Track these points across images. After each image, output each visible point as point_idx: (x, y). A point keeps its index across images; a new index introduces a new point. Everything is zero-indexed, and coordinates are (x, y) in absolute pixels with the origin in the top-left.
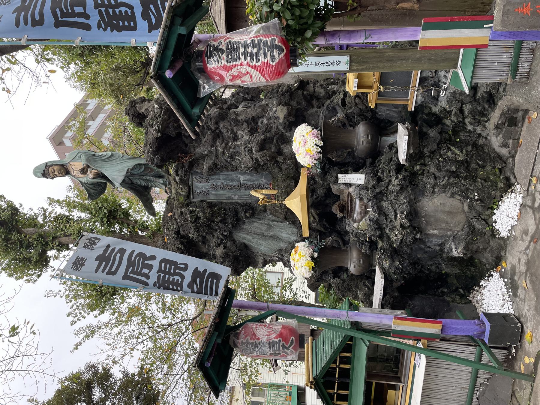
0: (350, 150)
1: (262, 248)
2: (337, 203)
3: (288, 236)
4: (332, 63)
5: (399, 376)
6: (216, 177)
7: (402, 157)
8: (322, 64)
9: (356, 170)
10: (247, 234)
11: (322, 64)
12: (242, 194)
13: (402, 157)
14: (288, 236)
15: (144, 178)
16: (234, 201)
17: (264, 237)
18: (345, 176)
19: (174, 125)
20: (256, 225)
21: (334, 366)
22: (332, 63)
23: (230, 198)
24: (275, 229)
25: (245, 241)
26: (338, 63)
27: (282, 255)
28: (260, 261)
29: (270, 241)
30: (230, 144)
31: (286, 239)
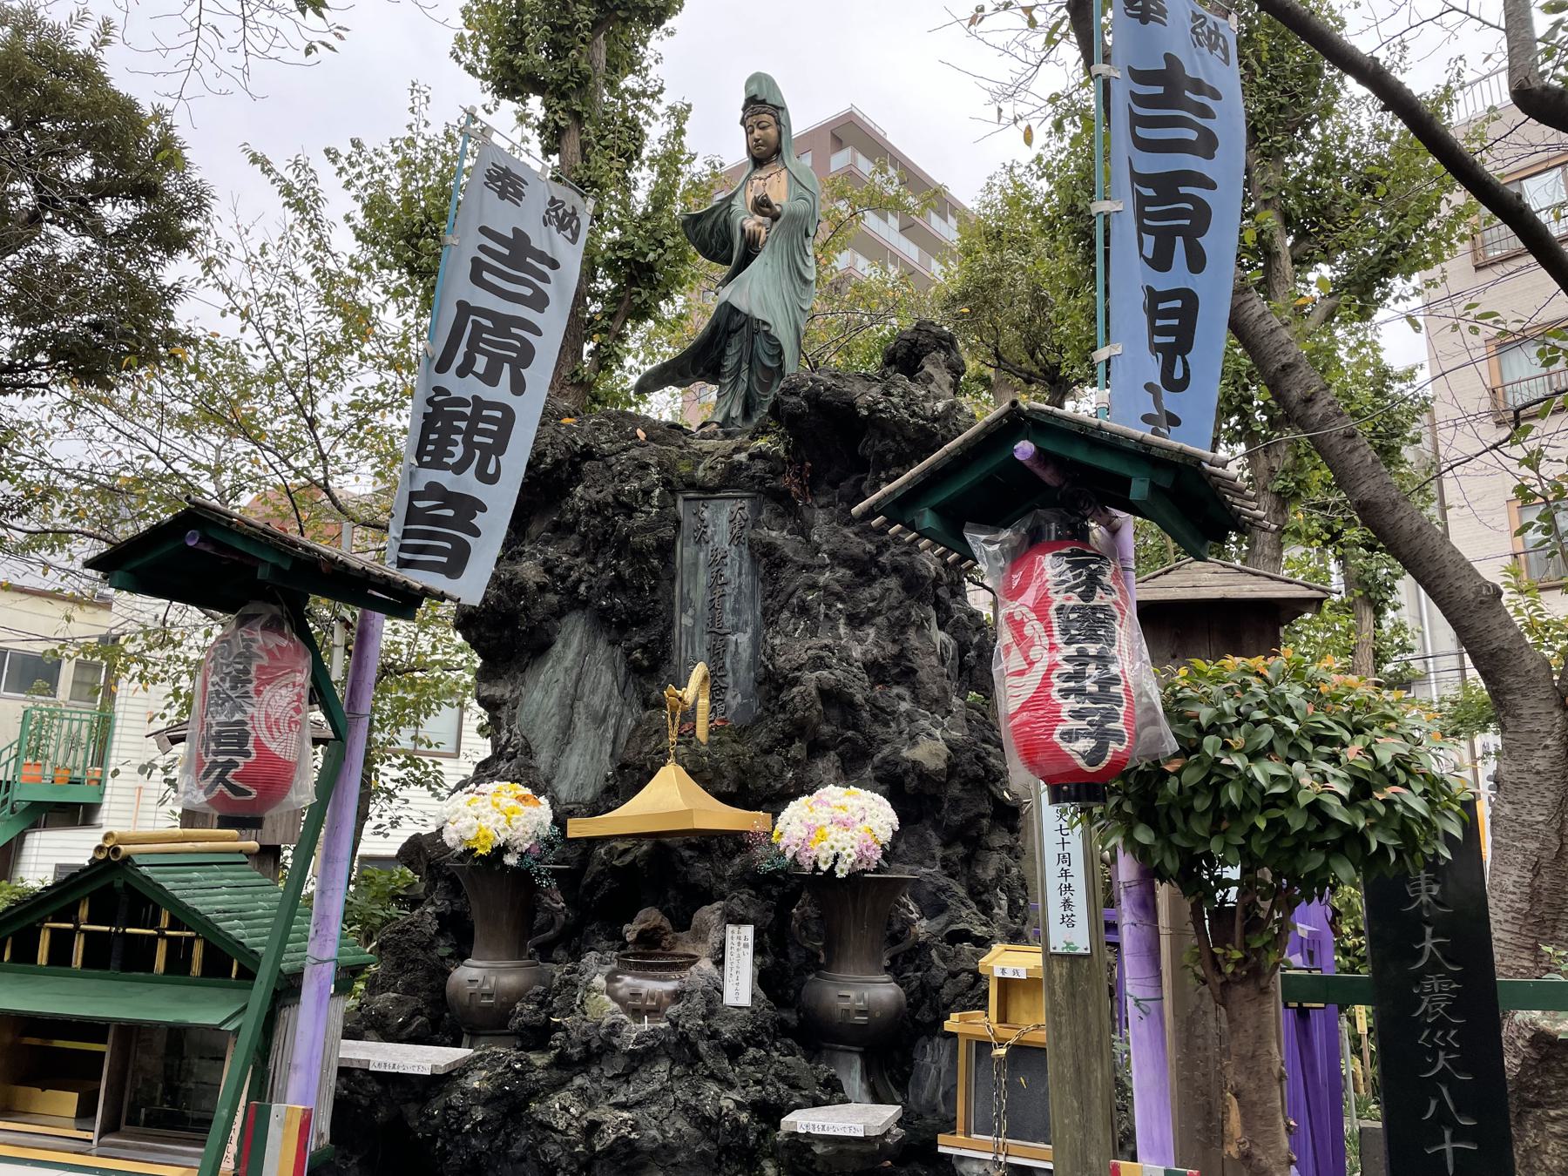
0: (822, 960)
1: (537, 695)
2: (666, 924)
3: (572, 772)
4: (1067, 904)
5: (123, 1127)
6: (746, 565)
7: (801, 1121)
8: (1065, 873)
9: (764, 979)
10: (579, 653)
11: (1065, 873)
12: (697, 639)
13: (801, 1121)
14: (572, 772)
15: (745, 366)
16: (677, 615)
17: (570, 702)
18: (746, 946)
19: (890, 451)
20: (607, 678)
21: (164, 921)
22: (1067, 904)
23: (687, 603)
24: (591, 733)
25: (558, 646)
26: (1068, 921)
28: (498, 691)
29: (556, 719)
30: (840, 606)
31: (563, 767)
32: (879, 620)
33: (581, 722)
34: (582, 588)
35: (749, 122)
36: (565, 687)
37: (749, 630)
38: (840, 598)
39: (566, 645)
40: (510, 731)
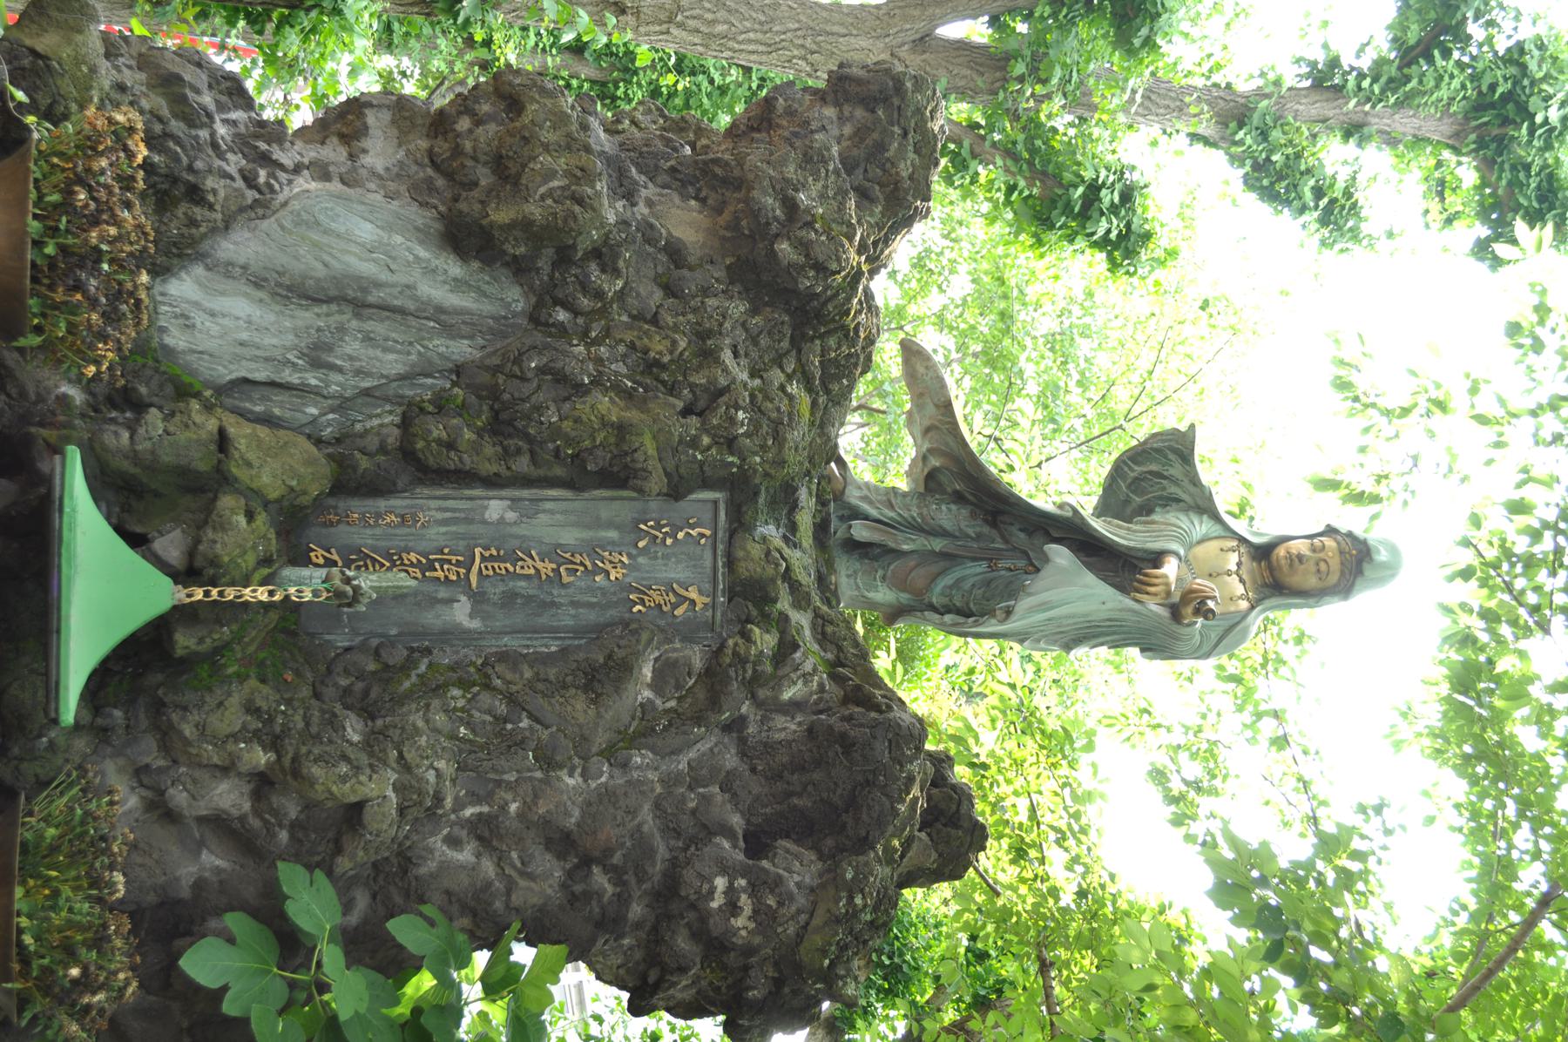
1: (366, 231)
6: (591, 617)
10: (440, 309)
12: (461, 529)
15: (938, 544)
16: (504, 493)
19: (780, 904)
20: (393, 364)
24: (289, 339)
25: (455, 268)
27: (250, 181)
28: (379, 152)
29: (320, 272)
30: (513, 807)
32: (488, 867)
33: (308, 317)
34: (562, 315)
35: (1329, 542)
36: (379, 285)
37: (475, 624)
38: (527, 808)
39: (458, 285)
40: (297, 169)
